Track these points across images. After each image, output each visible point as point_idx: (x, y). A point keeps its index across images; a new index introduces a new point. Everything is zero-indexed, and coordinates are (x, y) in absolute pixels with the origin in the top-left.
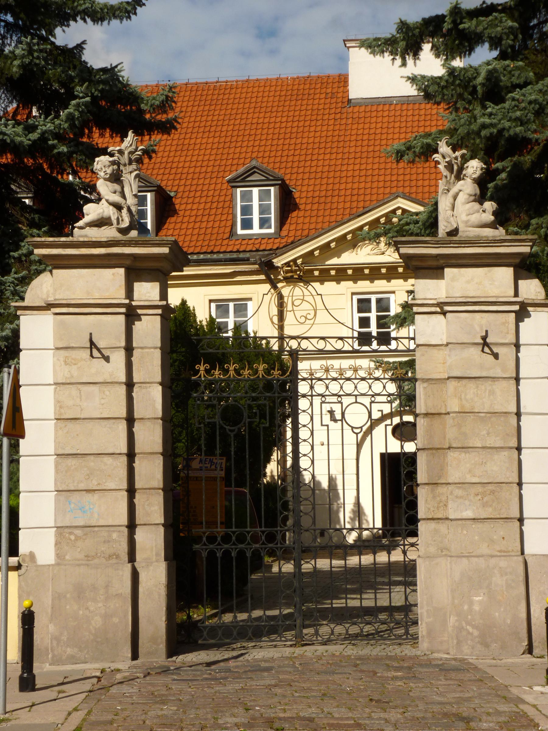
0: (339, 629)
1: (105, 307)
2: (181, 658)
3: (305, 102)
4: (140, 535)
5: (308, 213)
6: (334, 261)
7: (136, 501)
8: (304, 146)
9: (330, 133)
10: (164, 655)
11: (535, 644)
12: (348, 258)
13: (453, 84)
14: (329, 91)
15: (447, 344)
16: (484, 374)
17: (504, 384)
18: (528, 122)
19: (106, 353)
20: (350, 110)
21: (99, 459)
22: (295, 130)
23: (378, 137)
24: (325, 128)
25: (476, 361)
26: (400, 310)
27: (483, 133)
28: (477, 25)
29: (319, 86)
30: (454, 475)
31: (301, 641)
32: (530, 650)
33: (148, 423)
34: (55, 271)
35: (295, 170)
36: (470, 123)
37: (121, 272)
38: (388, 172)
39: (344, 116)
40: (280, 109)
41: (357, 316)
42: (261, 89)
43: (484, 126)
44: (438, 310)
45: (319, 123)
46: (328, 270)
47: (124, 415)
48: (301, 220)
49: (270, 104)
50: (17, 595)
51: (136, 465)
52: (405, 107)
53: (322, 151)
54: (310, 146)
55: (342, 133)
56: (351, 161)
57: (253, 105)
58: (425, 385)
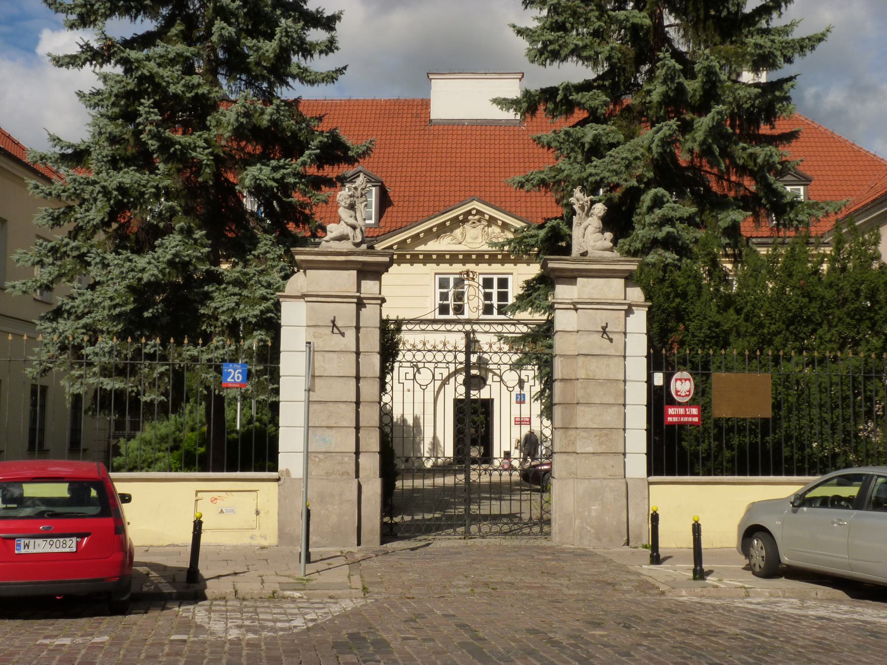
0: (495, 528)
1: (343, 298)
2: (389, 545)
3: (395, 120)
4: (362, 459)
5: (401, 209)
6: (422, 248)
7: (360, 435)
8: (396, 155)
9: (416, 146)
10: (379, 543)
11: (631, 539)
12: (433, 246)
13: (568, 141)
14: (414, 112)
15: (578, 332)
16: (603, 353)
17: (616, 360)
18: (621, 173)
19: (342, 330)
20: (431, 128)
21: (336, 405)
22: (388, 142)
23: (454, 150)
24: (412, 141)
25: (598, 343)
26: (515, 300)
27: (590, 179)
28: (582, 98)
29: (406, 107)
30: (581, 422)
31: (467, 535)
32: (628, 543)
33: (370, 381)
34: (308, 271)
35: (389, 174)
36: (582, 172)
37: (354, 273)
38: (463, 179)
39: (427, 132)
40: (376, 124)
41: (438, 291)
42: (360, 108)
43: (591, 175)
44: (572, 307)
45: (407, 137)
46: (418, 255)
47: (354, 375)
48: (395, 214)
49: (367, 120)
50: (277, 499)
51: (361, 410)
52: (474, 128)
53: (410, 160)
54: (401, 155)
55: (425, 146)
56: (434, 169)
57: (354, 120)
58: (562, 359)
